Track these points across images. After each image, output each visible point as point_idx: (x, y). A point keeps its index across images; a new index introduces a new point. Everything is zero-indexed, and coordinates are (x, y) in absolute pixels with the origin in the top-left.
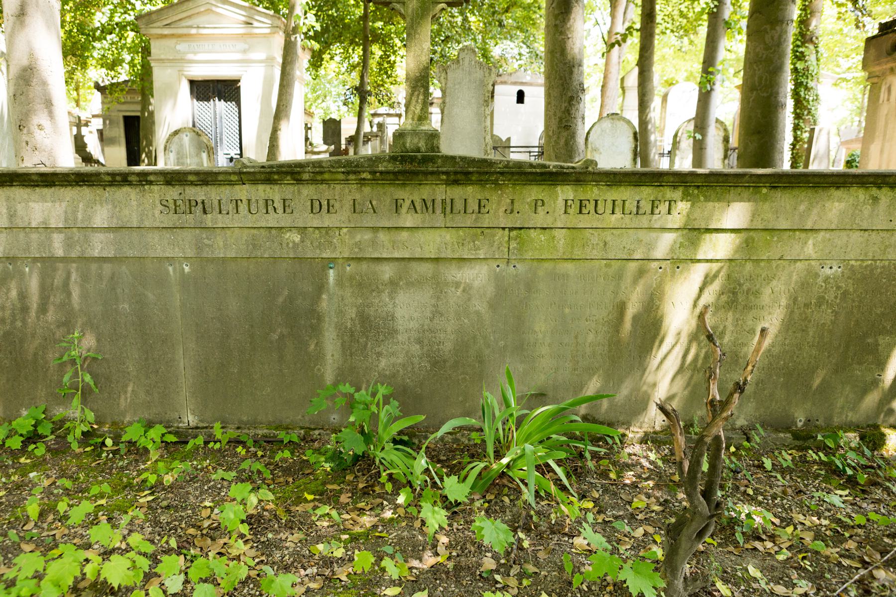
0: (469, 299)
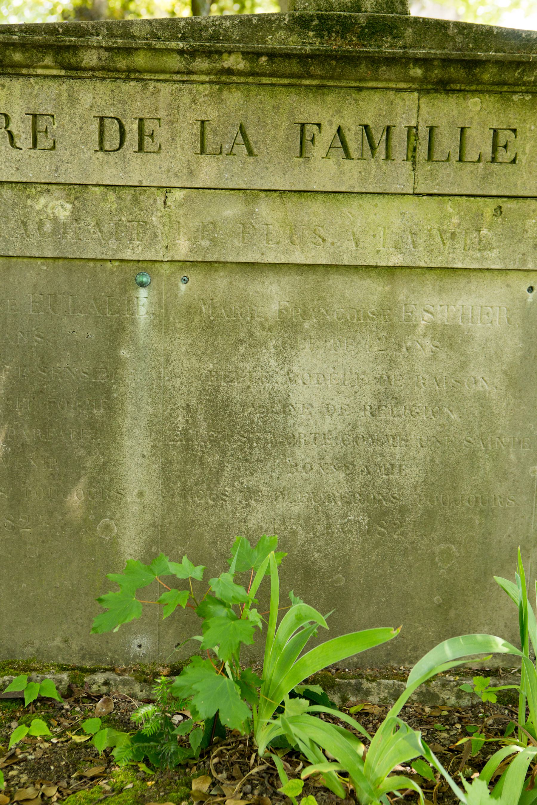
0: (463, 366)
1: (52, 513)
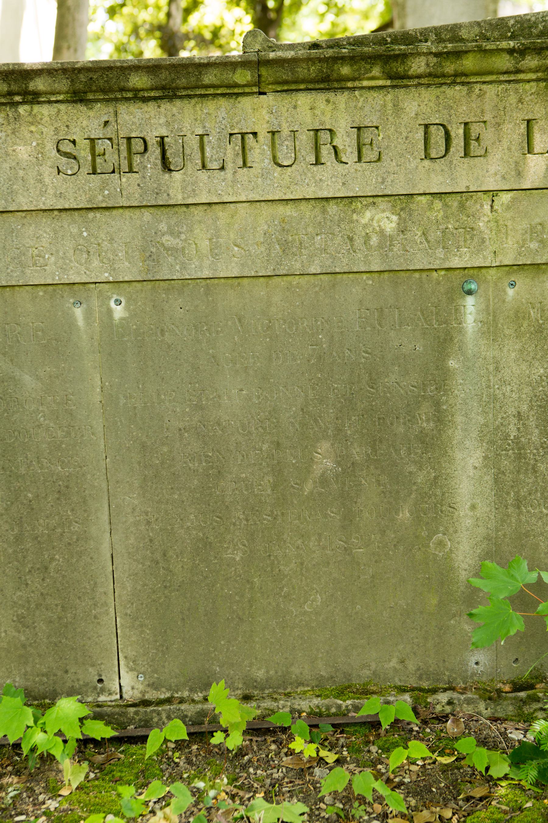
1: (385, 531)
